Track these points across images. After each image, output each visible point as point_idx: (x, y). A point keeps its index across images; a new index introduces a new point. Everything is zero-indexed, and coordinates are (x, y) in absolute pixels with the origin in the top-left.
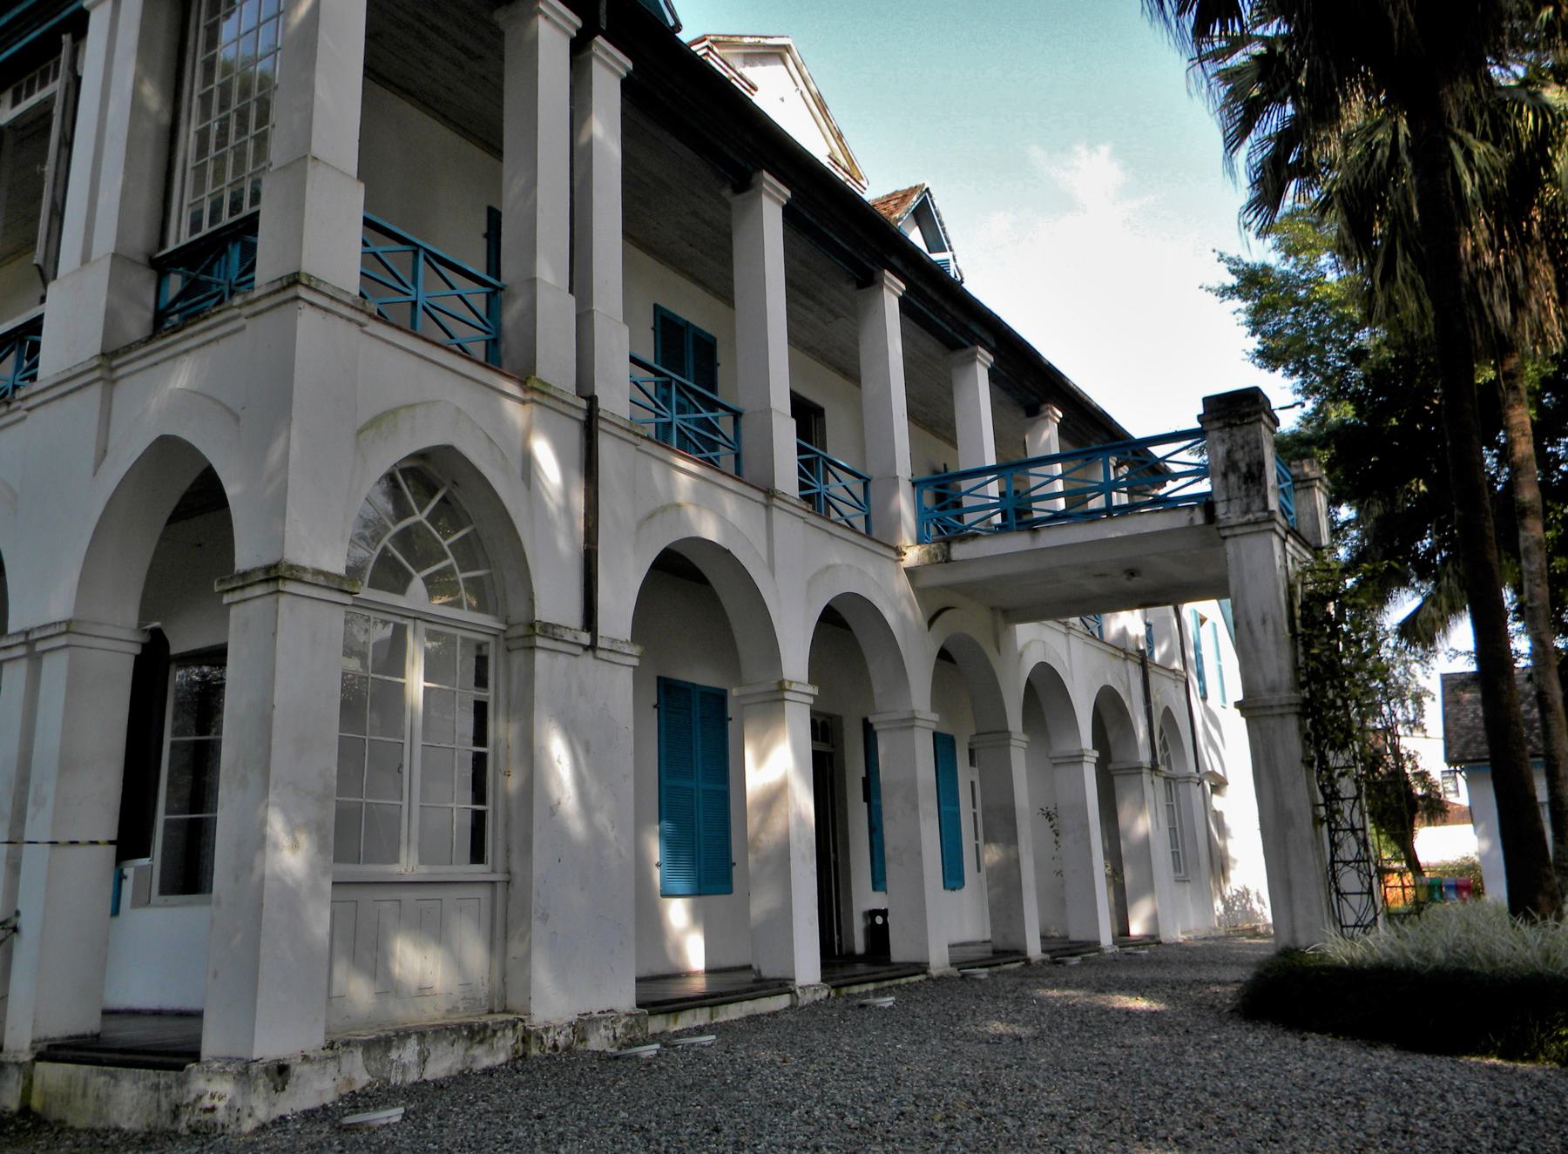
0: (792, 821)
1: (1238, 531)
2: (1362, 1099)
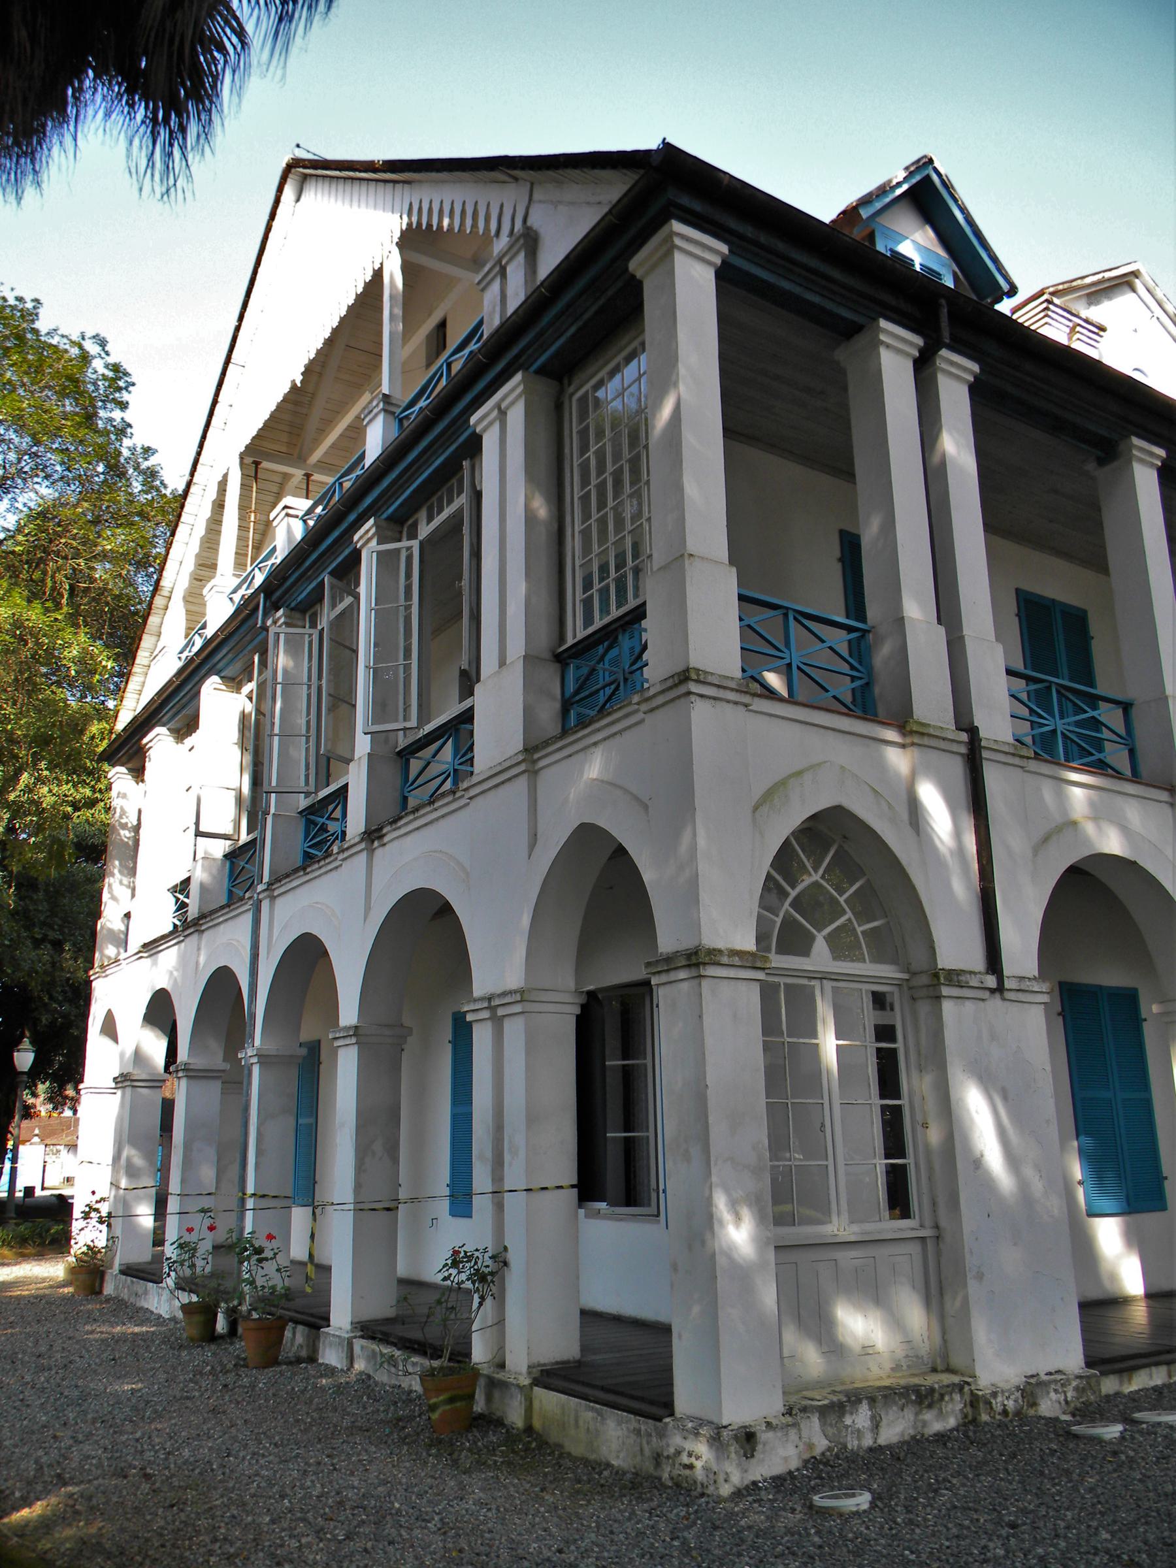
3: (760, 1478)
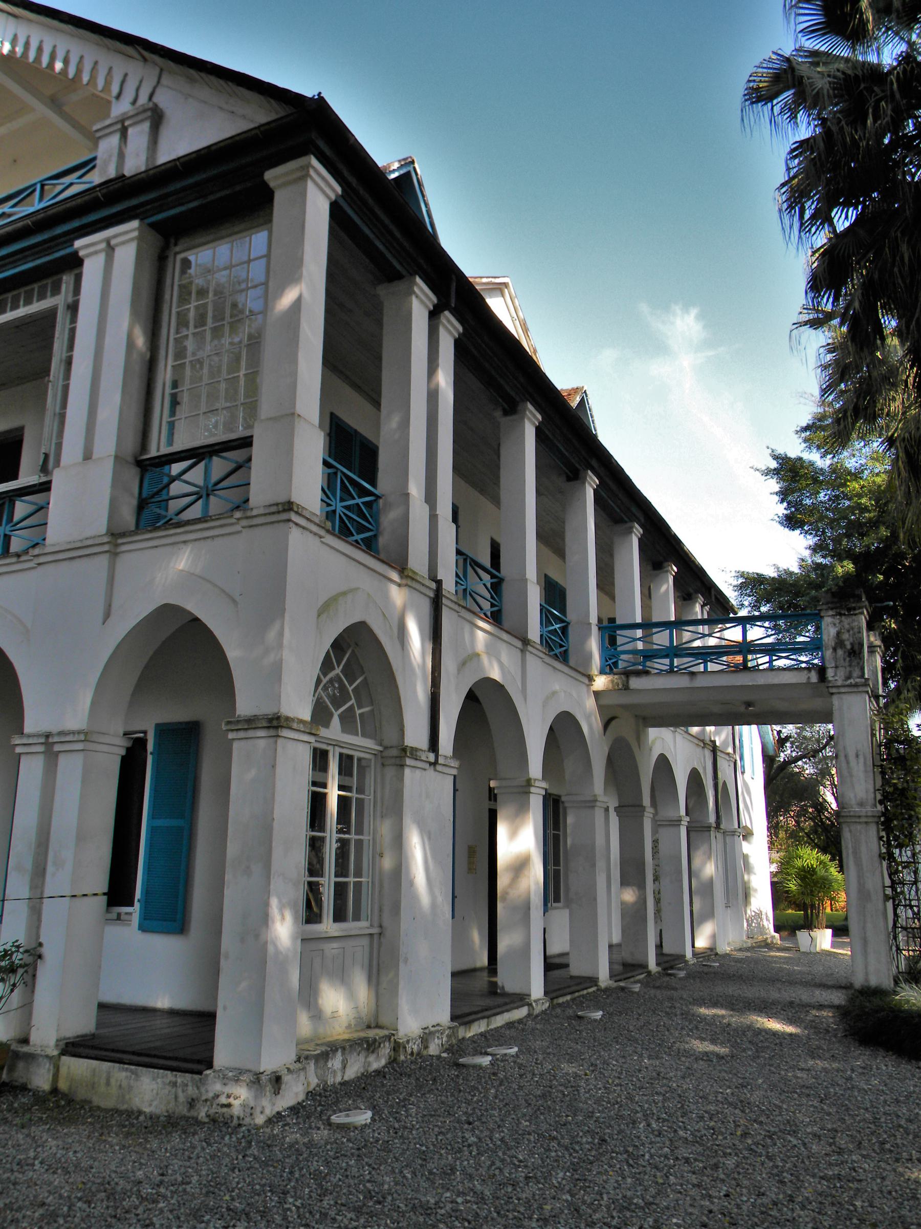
1: (843, 690)
3: (281, 1109)
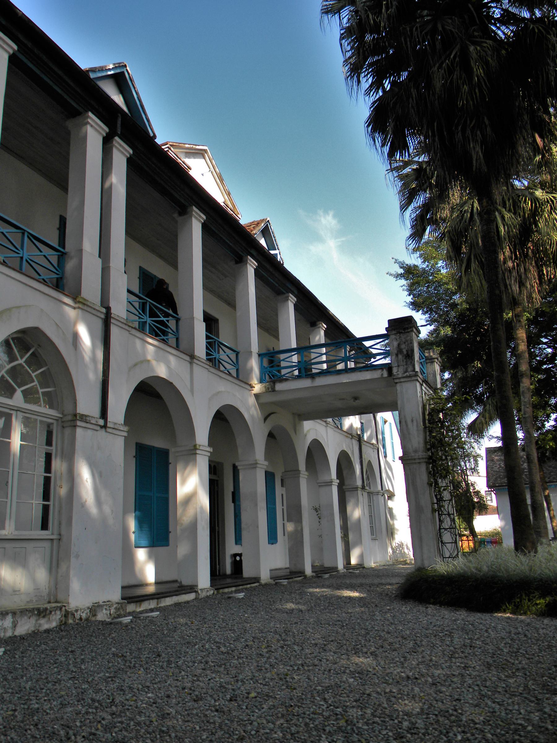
0: (198, 510)
1: (402, 380)
2: (452, 633)
